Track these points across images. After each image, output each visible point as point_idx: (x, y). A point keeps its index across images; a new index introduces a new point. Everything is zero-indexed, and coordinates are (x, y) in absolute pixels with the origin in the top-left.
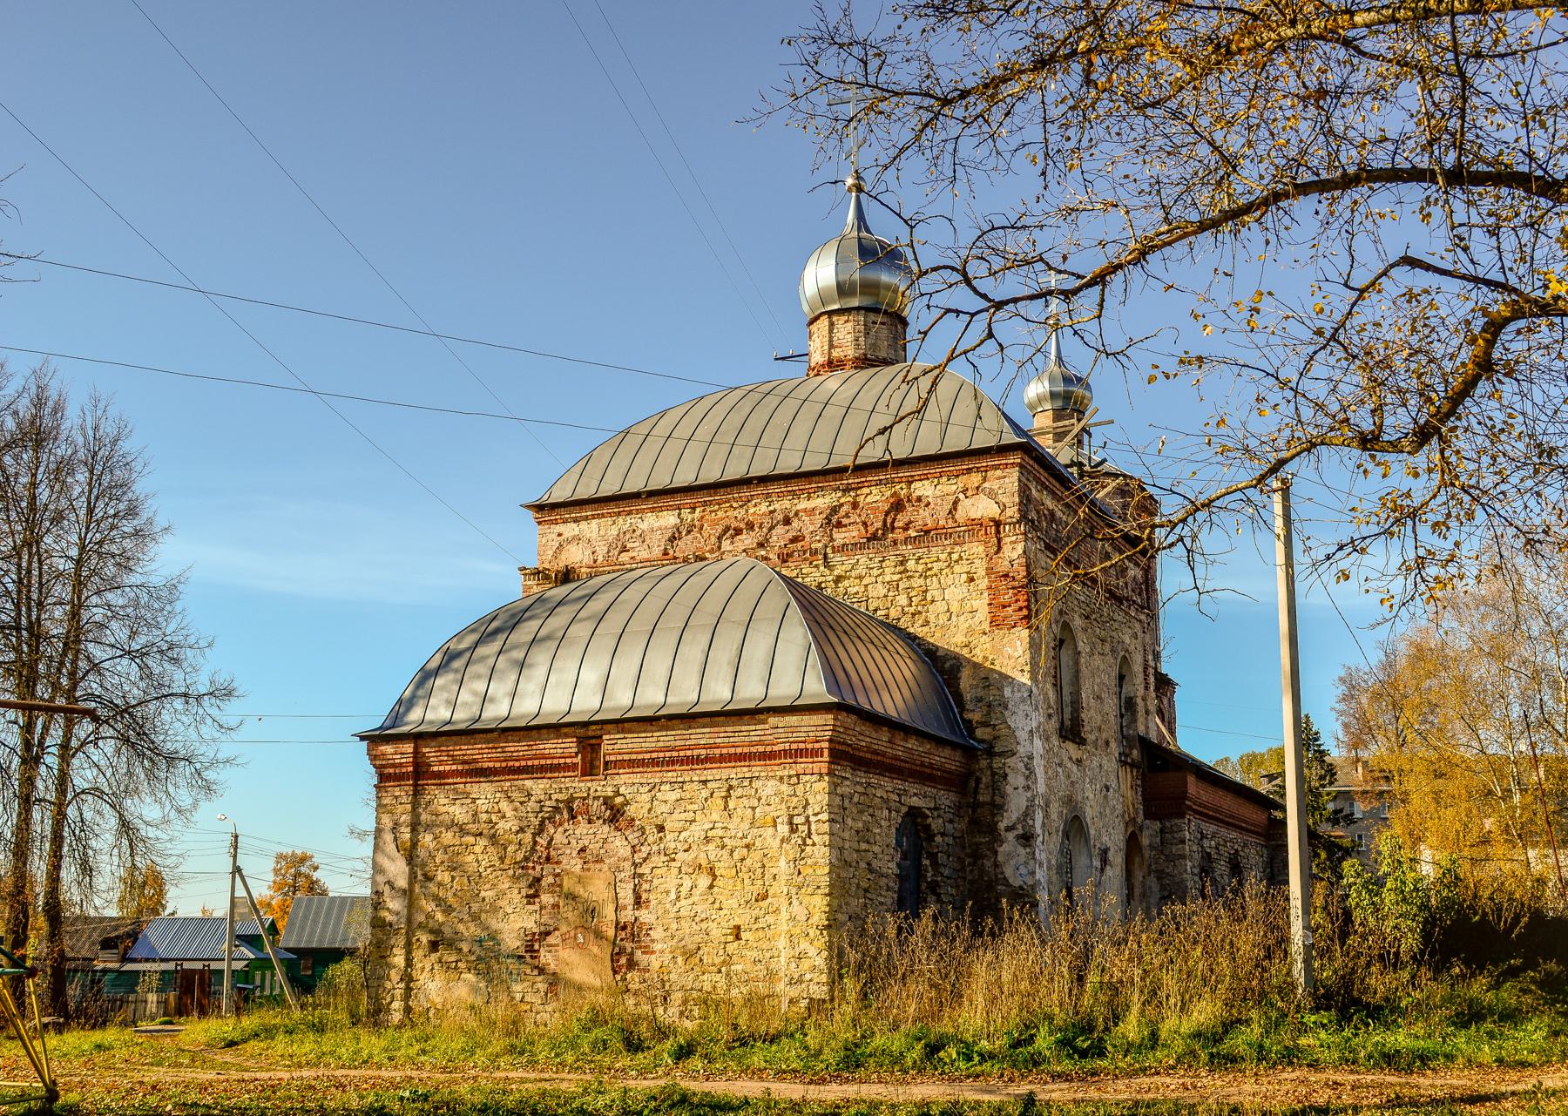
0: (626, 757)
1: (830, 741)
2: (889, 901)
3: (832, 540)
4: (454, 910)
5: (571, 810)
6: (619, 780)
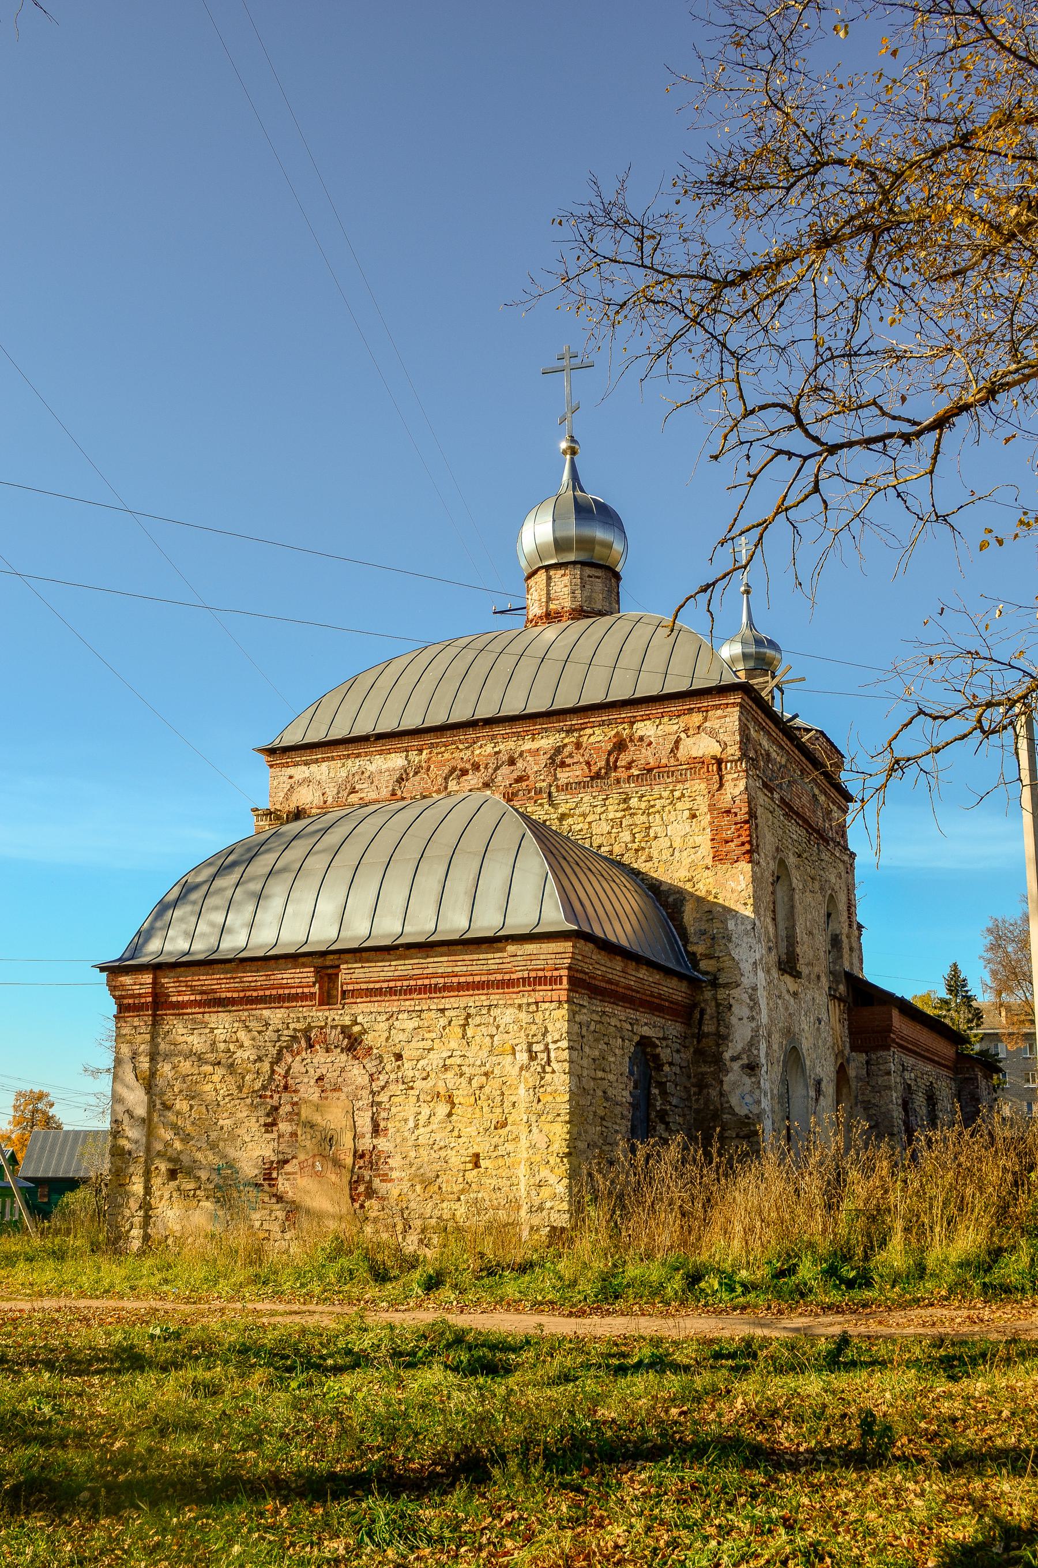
0: (364, 986)
1: (569, 968)
2: (624, 1129)
3: (556, 779)
4: (192, 1138)
5: (308, 1039)
6: (356, 1009)
